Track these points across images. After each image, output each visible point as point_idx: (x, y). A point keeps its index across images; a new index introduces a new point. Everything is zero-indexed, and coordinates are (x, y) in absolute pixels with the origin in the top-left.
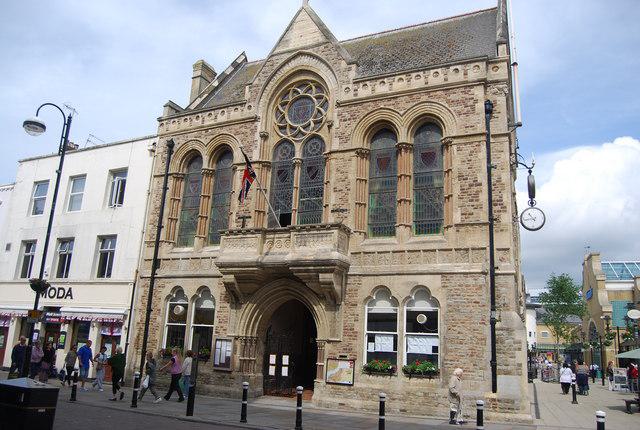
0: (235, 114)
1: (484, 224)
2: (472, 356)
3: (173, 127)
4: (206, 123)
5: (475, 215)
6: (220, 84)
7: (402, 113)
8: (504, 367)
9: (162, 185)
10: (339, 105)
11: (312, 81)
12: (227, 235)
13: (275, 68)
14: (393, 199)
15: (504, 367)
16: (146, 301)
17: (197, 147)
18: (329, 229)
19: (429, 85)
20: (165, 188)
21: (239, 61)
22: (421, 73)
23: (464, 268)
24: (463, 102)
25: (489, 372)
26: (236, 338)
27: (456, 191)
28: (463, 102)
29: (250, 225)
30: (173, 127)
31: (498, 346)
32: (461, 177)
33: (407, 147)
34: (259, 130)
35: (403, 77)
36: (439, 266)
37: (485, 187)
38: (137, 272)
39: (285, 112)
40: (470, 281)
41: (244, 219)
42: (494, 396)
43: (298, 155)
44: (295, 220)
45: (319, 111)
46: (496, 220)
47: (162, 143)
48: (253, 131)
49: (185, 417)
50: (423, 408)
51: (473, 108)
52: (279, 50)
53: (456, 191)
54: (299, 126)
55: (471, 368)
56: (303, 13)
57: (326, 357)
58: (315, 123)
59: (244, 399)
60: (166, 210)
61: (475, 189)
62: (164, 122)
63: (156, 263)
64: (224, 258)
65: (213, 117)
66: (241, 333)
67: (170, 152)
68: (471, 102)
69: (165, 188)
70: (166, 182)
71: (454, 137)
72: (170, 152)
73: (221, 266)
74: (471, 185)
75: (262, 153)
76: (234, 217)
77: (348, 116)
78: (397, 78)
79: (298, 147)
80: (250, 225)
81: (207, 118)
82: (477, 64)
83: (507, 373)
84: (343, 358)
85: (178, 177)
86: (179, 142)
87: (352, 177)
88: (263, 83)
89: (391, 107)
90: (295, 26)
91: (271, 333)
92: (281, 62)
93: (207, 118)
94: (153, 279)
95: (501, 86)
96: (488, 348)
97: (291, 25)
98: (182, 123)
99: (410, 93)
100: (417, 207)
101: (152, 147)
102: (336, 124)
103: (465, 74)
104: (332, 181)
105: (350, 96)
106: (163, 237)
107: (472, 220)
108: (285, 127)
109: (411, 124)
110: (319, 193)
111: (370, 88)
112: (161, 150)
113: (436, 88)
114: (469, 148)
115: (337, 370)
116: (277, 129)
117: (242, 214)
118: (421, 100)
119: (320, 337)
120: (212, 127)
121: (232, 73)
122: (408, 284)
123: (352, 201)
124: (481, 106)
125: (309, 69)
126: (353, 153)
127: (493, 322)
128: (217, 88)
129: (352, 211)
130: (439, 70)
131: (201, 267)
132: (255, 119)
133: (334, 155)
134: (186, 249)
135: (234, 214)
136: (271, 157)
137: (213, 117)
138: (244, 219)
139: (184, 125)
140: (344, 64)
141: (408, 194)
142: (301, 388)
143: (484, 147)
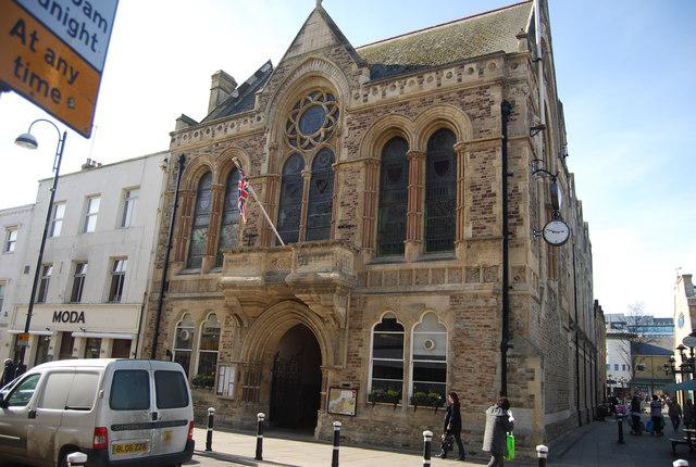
1: (498, 239)
11: (323, 88)
15: (515, 399)
24: (479, 104)
27: (469, 203)
32: (474, 187)
37: (499, 198)
48: (263, 143)
51: (488, 109)
52: (291, 55)
53: (469, 203)
55: (479, 398)
58: (327, 133)
60: (177, 230)
63: (165, 286)
67: (182, 168)
72: (182, 168)
75: (271, 168)
84: (346, 387)
87: (360, 189)
90: (308, 28)
92: (294, 67)
96: (498, 377)
97: (303, 28)
103: (481, 73)
110: (329, 208)
115: (339, 400)
116: (287, 141)
117: (248, 232)
121: (255, 83)
124: (497, 108)
126: (361, 164)
128: (237, 99)
130: (453, 70)
143: (499, 154)
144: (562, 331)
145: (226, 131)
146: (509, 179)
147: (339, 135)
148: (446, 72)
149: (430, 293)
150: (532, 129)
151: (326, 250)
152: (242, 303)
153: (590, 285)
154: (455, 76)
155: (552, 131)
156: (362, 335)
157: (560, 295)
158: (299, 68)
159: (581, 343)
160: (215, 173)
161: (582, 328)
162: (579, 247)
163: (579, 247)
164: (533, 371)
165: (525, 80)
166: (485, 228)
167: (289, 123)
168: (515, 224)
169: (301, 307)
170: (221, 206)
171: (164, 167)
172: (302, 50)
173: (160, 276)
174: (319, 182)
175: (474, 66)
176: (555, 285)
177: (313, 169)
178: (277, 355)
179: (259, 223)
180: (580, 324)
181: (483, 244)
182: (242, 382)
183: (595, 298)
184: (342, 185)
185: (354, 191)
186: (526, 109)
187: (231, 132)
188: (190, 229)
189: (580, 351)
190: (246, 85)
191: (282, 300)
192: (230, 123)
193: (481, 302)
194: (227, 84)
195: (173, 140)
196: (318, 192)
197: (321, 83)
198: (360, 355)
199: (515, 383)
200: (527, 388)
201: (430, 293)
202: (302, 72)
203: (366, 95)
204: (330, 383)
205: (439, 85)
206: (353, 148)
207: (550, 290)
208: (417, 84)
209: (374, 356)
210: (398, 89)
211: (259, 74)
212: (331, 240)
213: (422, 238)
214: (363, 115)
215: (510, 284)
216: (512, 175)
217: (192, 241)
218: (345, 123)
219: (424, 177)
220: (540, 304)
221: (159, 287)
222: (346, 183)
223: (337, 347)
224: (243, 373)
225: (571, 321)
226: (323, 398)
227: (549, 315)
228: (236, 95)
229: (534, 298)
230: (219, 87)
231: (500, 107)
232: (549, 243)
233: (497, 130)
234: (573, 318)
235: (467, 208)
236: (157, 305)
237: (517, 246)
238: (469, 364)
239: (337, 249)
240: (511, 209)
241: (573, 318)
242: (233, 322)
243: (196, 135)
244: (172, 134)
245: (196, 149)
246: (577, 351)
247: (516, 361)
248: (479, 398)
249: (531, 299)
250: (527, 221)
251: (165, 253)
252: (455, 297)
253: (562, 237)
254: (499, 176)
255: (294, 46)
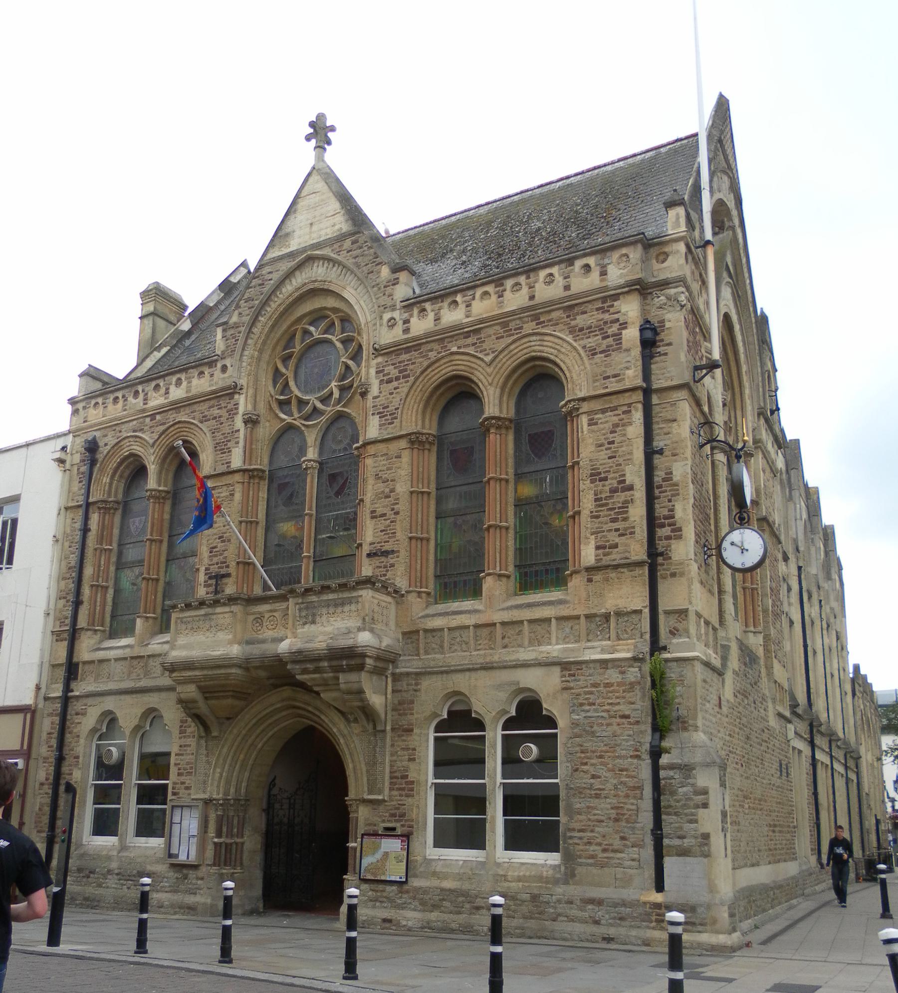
0: (200, 384)
1: (640, 564)
2: (617, 820)
3: (95, 415)
4: (152, 403)
5: (620, 548)
6: (195, 325)
7: (488, 359)
8: (677, 842)
9: (78, 525)
10: (378, 351)
11: (335, 310)
12: (182, 610)
13: (267, 289)
14: (477, 526)
15: (677, 842)
16: (54, 743)
17: (137, 449)
18: (354, 588)
19: (537, 300)
20: (85, 530)
21: (234, 279)
22: (522, 279)
23: (603, 651)
24: (600, 329)
25: (648, 853)
26: (207, 802)
27: (587, 504)
28: (600, 329)
29: (230, 589)
30: (95, 415)
31: (664, 801)
32: (597, 476)
33: (499, 423)
34: (241, 409)
35: (490, 288)
36: (555, 649)
37: (640, 494)
38: (38, 688)
39: (290, 374)
40: (613, 676)
41: (218, 578)
42: (658, 898)
43: (312, 453)
44: (307, 575)
45: (347, 367)
46: (662, 554)
47: (75, 444)
48: (233, 412)
49: (44, 948)
50: (532, 924)
51: (618, 337)
52: (275, 253)
53: (587, 504)
54: (313, 399)
55: (617, 843)
56: (315, 177)
57: (361, 831)
58: (342, 389)
59: (496, 938)
60: (88, 571)
61: (621, 497)
62: (80, 406)
63: (72, 670)
64: (177, 654)
65: (163, 390)
66: (218, 795)
67: (93, 462)
68: (615, 328)
69: (85, 530)
70: (86, 518)
71: (583, 399)
72: (93, 462)
73: (172, 668)
74: (614, 491)
75: (249, 453)
76: (202, 577)
77: (394, 373)
78: (479, 292)
79: (312, 438)
80: (230, 589)
81: (152, 394)
82: (624, 251)
83: (684, 853)
84: (390, 832)
85: (105, 508)
86: (107, 441)
87: (402, 488)
88: (246, 319)
89: (471, 350)
90: (301, 204)
91: (275, 791)
92: (276, 276)
93: (152, 394)
94: (66, 700)
95: (672, 291)
96: (647, 804)
97: (294, 203)
98: (110, 407)
99: (504, 321)
100: (521, 538)
101: (58, 455)
102: (374, 390)
103: (603, 273)
104: (368, 497)
105: (397, 334)
106: (82, 622)
107: (615, 557)
108: (288, 402)
109: (514, 370)
110: (350, 523)
111: (431, 316)
112: (77, 458)
113: (550, 305)
114: (611, 418)
115: (378, 856)
116: (275, 406)
117: (214, 569)
118: (525, 332)
119: (352, 794)
120: (162, 410)
121: (219, 303)
122: (499, 687)
123: (402, 535)
124: (632, 335)
125: (316, 285)
126: (403, 443)
127: (656, 753)
128: (189, 333)
129: (403, 554)
130: (555, 270)
131: (147, 674)
132: (233, 390)
133: (371, 449)
134: (124, 642)
135: (202, 569)
136: (266, 460)
137: (163, 390)
138: (218, 578)
139: (115, 411)
140: (385, 271)
141: (503, 516)
142: (229, 884)
143: (638, 416)
144: (773, 722)
145: (167, 393)
146: (657, 460)
147: (364, 394)
148: (542, 274)
149: (525, 665)
150: (697, 368)
151: (346, 595)
152: (207, 692)
153: (840, 637)
154: (559, 281)
155: (744, 368)
156: (414, 740)
157: (768, 657)
158: (289, 275)
159: (818, 740)
160: (152, 469)
161: (823, 717)
162: (814, 569)
163: (814, 569)
164: (705, 792)
165: (682, 281)
166: (616, 546)
167: (277, 373)
168: (668, 538)
169: (307, 697)
170: (166, 525)
171: (61, 461)
172: (294, 245)
173: (62, 655)
174: (333, 477)
175: (591, 261)
176: (755, 642)
177: (321, 453)
178: (272, 784)
179: (232, 549)
180: (820, 705)
181: (613, 575)
182: (212, 832)
183: (852, 661)
184: (371, 481)
185: (392, 491)
186: (685, 334)
187: (177, 393)
188: (112, 568)
189: (819, 756)
190: (203, 311)
191: (276, 686)
192: (174, 379)
193: (613, 676)
194: (167, 310)
195: (75, 412)
196: (332, 494)
197: (330, 302)
198: (412, 776)
199: (676, 814)
200: (696, 821)
201: (525, 665)
202: (289, 288)
203: (406, 322)
204: (361, 831)
205: (532, 298)
206: (387, 415)
207: (744, 648)
208: (494, 297)
209: (504, 777)
210: (462, 307)
211: (226, 287)
212: (355, 578)
213: (511, 568)
214: (404, 357)
215: (662, 642)
216: (661, 452)
217: (117, 591)
218: (373, 371)
219: (511, 462)
220: (720, 674)
221: (61, 673)
222: (377, 477)
223: (372, 764)
224: (212, 817)
225: (794, 706)
226: (351, 853)
227: (741, 693)
228: (186, 326)
229: (707, 664)
230: (154, 314)
231: (638, 334)
232: (734, 569)
233: (633, 376)
234: (801, 698)
235: (585, 514)
236: (58, 706)
237: (673, 575)
238: (597, 784)
239: (366, 594)
240: (661, 511)
241: (801, 698)
242: (192, 728)
243: (116, 400)
244: (72, 401)
245: (114, 425)
246: (814, 762)
247: (677, 775)
248: (617, 843)
249: (698, 667)
250: (690, 532)
251: (69, 613)
252: (567, 666)
253: (752, 557)
254: (639, 455)
255: (280, 235)
